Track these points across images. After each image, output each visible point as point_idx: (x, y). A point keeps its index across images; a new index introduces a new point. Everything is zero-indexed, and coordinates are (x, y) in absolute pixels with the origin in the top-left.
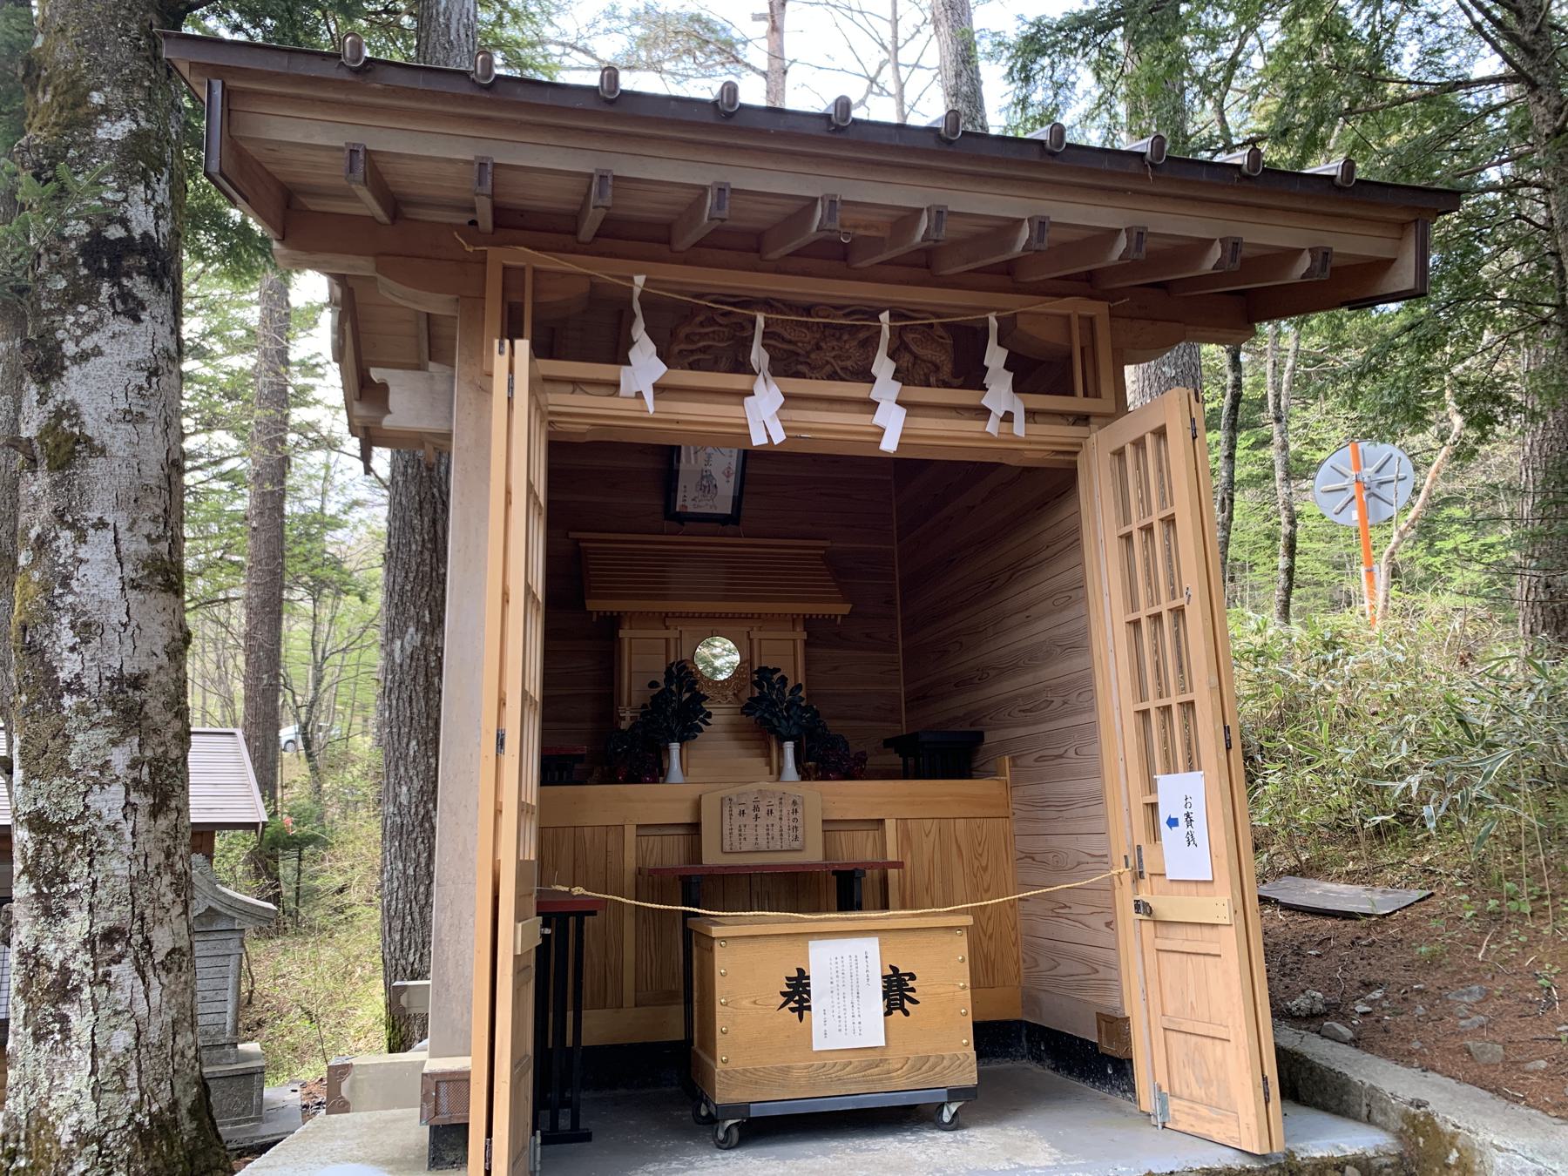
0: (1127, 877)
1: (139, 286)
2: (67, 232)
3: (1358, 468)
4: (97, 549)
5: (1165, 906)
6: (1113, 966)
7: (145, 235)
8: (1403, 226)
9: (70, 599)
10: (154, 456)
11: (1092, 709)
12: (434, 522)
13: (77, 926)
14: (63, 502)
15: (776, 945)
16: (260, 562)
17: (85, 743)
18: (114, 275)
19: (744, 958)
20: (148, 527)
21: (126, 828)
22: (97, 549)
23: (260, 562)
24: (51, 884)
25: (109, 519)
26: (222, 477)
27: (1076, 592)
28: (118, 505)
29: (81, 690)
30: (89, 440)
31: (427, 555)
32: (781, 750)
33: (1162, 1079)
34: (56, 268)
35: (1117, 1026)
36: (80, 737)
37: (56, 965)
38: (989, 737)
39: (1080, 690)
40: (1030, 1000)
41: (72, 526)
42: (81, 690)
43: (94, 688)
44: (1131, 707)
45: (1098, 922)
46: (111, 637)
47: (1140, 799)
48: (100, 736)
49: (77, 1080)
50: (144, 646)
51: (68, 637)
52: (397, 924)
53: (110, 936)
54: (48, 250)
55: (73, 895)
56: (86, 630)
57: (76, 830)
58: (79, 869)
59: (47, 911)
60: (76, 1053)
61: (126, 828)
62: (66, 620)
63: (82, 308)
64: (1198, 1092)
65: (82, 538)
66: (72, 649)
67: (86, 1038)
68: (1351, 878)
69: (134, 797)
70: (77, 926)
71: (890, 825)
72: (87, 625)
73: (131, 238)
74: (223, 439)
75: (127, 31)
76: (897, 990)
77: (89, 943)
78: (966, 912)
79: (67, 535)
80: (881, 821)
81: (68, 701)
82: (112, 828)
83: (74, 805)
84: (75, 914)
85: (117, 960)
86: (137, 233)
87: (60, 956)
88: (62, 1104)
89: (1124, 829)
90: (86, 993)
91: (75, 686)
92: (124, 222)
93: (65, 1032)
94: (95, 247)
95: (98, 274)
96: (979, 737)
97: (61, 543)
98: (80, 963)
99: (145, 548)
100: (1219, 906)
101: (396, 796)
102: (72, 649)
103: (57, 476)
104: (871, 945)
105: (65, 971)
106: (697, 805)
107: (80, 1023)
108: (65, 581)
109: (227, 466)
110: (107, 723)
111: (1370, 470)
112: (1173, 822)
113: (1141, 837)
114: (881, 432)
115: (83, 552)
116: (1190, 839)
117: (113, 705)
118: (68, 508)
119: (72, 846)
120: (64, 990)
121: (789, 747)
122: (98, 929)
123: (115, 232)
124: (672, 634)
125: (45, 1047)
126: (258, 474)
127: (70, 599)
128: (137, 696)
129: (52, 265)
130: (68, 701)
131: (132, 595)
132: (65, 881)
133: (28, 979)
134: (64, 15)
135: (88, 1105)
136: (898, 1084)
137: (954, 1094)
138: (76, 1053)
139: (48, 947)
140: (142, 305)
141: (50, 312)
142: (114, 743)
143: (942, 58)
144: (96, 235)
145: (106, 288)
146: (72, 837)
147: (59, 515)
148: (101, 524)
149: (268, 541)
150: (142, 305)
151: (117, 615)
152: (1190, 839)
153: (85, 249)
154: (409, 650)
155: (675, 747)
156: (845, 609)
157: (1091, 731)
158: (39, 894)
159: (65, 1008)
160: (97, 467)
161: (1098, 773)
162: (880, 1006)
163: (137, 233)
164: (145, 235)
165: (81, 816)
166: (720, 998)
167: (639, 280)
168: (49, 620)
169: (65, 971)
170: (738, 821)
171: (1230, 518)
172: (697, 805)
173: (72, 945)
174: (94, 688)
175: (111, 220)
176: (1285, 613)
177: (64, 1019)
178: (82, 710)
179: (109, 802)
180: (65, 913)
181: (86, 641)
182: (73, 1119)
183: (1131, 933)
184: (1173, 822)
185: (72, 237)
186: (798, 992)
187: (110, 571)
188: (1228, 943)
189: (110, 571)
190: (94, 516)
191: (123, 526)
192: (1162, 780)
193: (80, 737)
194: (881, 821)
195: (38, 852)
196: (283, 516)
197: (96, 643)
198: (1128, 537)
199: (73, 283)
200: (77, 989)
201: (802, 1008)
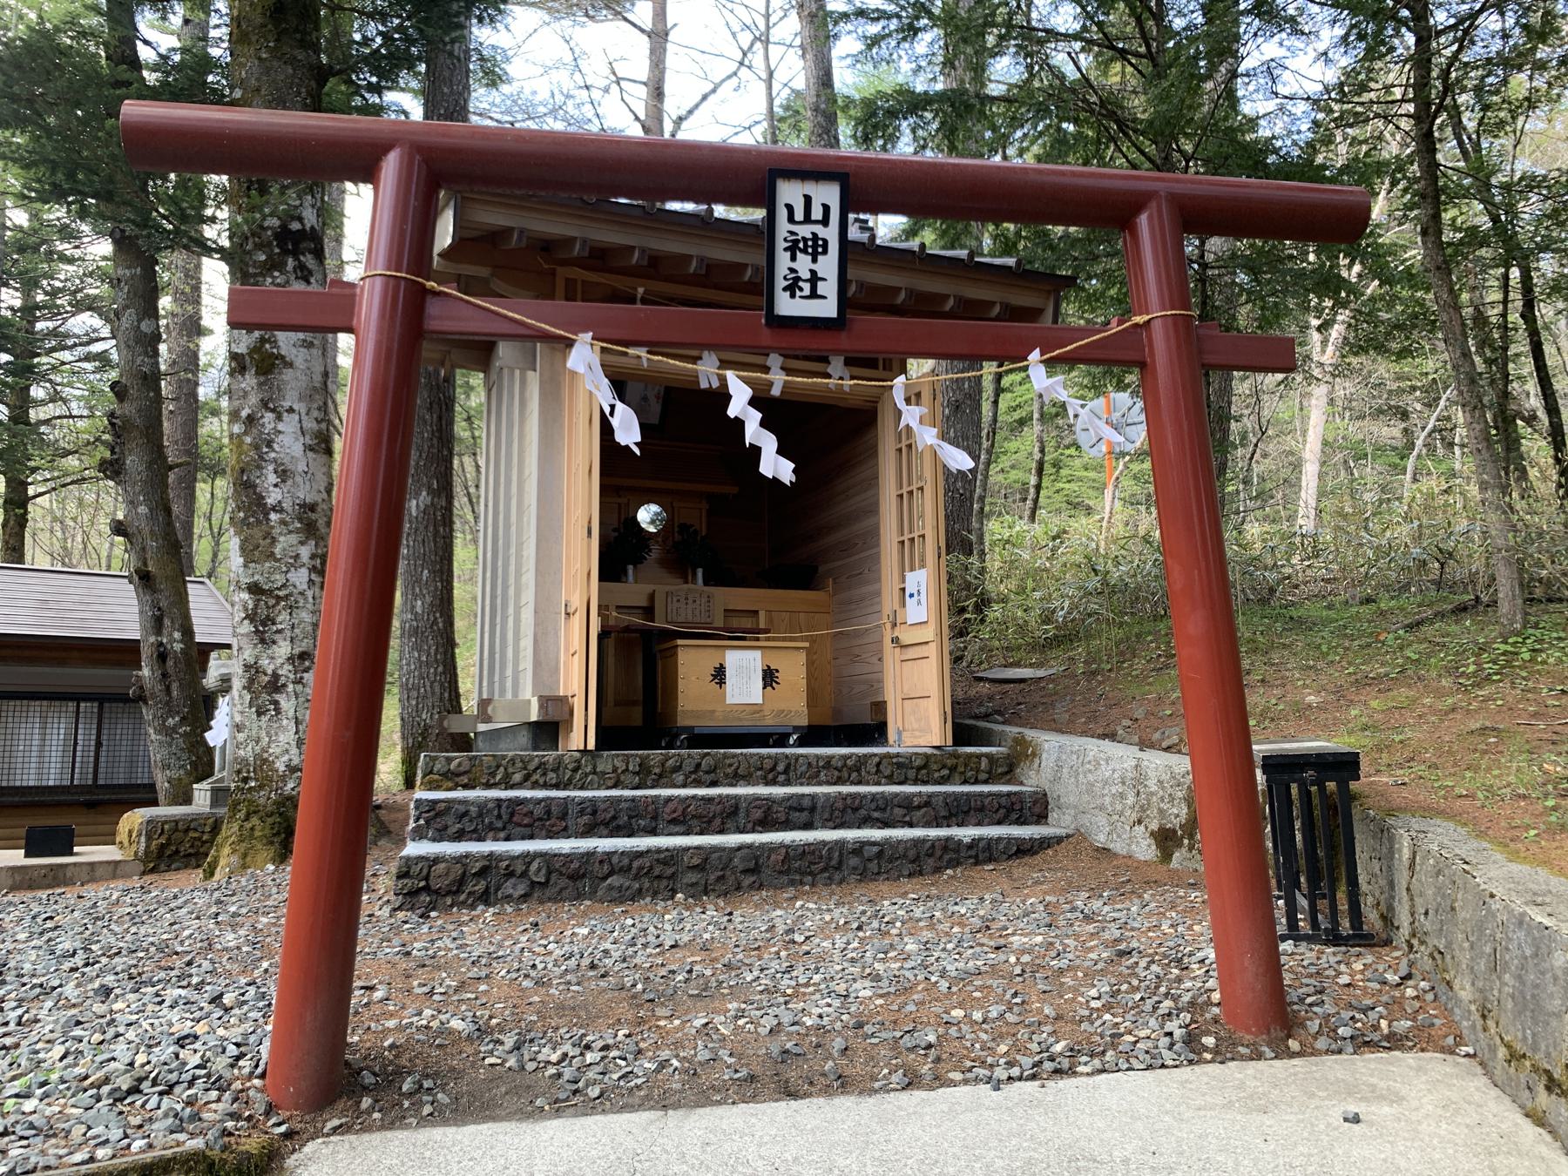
0: (889, 626)
1: (309, 260)
2: (266, 224)
3: (1109, 412)
4: (289, 425)
5: (906, 638)
6: (881, 681)
7: (312, 228)
8: (1049, 292)
9: (273, 455)
10: (318, 369)
11: (878, 545)
12: (440, 418)
13: (283, 649)
14: (266, 396)
15: (712, 651)
16: (176, 443)
17: (285, 542)
18: (295, 254)
19: (692, 663)
20: (316, 414)
21: (310, 594)
22: (289, 425)
23: (176, 443)
24: (264, 625)
25: (296, 407)
26: (88, 358)
27: (873, 481)
28: (300, 400)
29: (281, 511)
30: (283, 357)
31: (435, 441)
32: (694, 575)
33: (900, 724)
34: (259, 247)
35: (880, 707)
36: (282, 539)
37: (270, 672)
38: (821, 569)
39: (874, 535)
40: (837, 712)
41: (273, 411)
42: (281, 511)
43: (290, 510)
44: (896, 539)
45: (874, 660)
46: (299, 479)
47: (897, 587)
48: (293, 539)
49: (287, 736)
50: (315, 487)
51: (272, 478)
52: (415, 694)
53: (304, 656)
54: (253, 235)
55: (279, 632)
56: (284, 474)
57: (281, 593)
58: (283, 617)
59: (263, 641)
60: (285, 722)
61: (310, 594)
62: (271, 468)
63: (276, 274)
64: (916, 726)
65: (279, 418)
66: (276, 485)
67: (291, 713)
68: (1031, 666)
69: (313, 576)
70: (283, 649)
71: (762, 614)
72: (284, 471)
73: (304, 230)
74: (84, 322)
75: (299, 93)
76: (769, 677)
77: (291, 659)
78: (802, 639)
79: (269, 416)
80: (756, 612)
81: (273, 516)
82: (301, 594)
83: (279, 579)
84: (281, 643)
85: (306, 670)
86: (308, 227)
87: (272, 667)
88: (278, 751)
89: (889, 601)
90: (291, 687)
91: (277, 508)
92: (300, 219)
93: (278, 710)
94: (283, 235)
95: (285, 252)
96: (815, 569)
97: (265, 420)
98: (286, 671)
99: (315, 426)
100: (929, 633)
101: (413, 607)
102: (276, 485)
103: (262, 379)
104: (758, 654)
105: (276, 676)
106: (652, 597)
107: (287, 704)
108: (269, 444)
109: (97, 348)
110: (298, 531)
111: (1118, 414)
112: (911, 596)
113: (896, 606)
114: (771, 384)
115: (280, 427)
116: (919, 602)
117: (300, 520)
118: (271, 399)
119: (278, 603)
120: (275, 686)
121: (700, 572)
122: (297, 651)
123: (295, 226)
124: (623, 500)
125: (264, 719)
126: (174, 362)
127: (273, 455)
128: (313, 516)
129: (255, 245)
130: (273, 516)
131: (310, 454)
132: (274, 623)
133: (251, 681)
134: (258, 79)
135: (294, 751)
136: (769, 722)
137: (796, 729)
138: (285, 722)
139: (264, 662)
140: (310, 273)
141: (255, 275)
142: (302, 543)
143: (807, 79)
144: (284, 227)
145: (291, 263)
146: (279, 598)
147: (265, 404)
148: (291, 410)
149: (185, 423)
150: (310, 273)
151: (302, 467)
152: (919, 602)
153: (277, 236)
154: (422, 507)
155: (630, 568)
156: (735, 490)
157: (876, 559)
158: (257, 631)
159: (277, 697)
160: (288, 374)
161: (878, 580)
162: (760, 684)
163: (308, 227)
164: (312, 228)
165: (284, 586)
166: (681, 676)
167: (641, 290)
168: (260, 467)
169: (276, 676)
170: (676, 605)
171: (993, 445)
172: (652, 597)
173: (280, 661)
174: (290, 510)
175: (293, 218)
176: (1032, 518)
177: (276, 703)
178: (283, 522)
179: (300, 578)
180: (274, 642)
181: (284, 481)
182: (286, 758)
183: (890, 654)
184: (911, 596)
185: (268, 228)
186: (719, 675)
187: (297, 439)
188: (932, 651)
189: (297, 439)
190: (286, 404)
191: (303, 412)
192: (909, 575)
193: (282, 539)
194: (756, 612)
195: (256, 606)
196: (197, 401)
197: (290, 482)
198: (900, 450)
199: (270, 257)
200: (284, 685)
201: (722, 682)
